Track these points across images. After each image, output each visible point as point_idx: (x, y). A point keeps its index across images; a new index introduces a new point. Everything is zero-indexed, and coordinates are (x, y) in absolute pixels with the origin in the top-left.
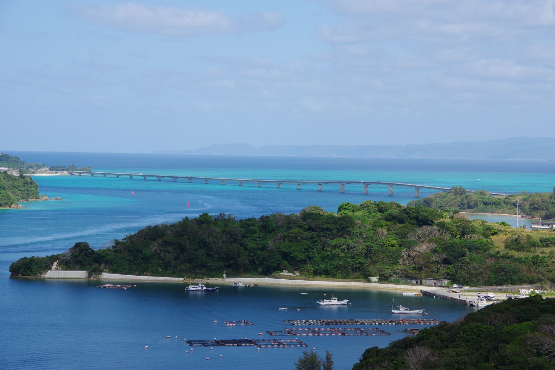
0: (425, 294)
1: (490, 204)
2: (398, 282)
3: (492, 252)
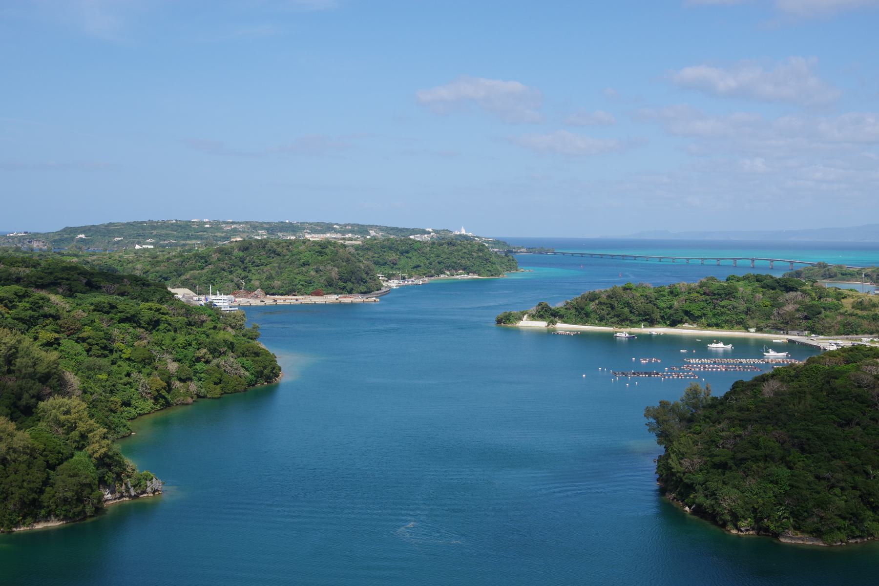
0: (790, 341)
1: (846, 274)
2: (770, 333)
3: (841, 311)
